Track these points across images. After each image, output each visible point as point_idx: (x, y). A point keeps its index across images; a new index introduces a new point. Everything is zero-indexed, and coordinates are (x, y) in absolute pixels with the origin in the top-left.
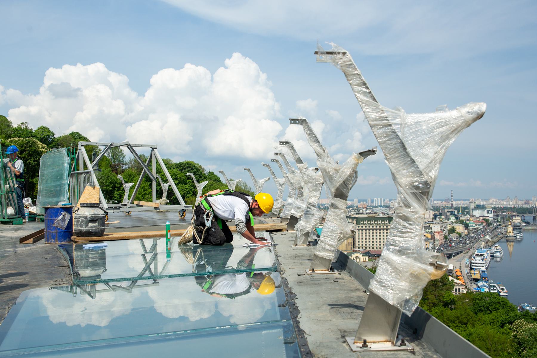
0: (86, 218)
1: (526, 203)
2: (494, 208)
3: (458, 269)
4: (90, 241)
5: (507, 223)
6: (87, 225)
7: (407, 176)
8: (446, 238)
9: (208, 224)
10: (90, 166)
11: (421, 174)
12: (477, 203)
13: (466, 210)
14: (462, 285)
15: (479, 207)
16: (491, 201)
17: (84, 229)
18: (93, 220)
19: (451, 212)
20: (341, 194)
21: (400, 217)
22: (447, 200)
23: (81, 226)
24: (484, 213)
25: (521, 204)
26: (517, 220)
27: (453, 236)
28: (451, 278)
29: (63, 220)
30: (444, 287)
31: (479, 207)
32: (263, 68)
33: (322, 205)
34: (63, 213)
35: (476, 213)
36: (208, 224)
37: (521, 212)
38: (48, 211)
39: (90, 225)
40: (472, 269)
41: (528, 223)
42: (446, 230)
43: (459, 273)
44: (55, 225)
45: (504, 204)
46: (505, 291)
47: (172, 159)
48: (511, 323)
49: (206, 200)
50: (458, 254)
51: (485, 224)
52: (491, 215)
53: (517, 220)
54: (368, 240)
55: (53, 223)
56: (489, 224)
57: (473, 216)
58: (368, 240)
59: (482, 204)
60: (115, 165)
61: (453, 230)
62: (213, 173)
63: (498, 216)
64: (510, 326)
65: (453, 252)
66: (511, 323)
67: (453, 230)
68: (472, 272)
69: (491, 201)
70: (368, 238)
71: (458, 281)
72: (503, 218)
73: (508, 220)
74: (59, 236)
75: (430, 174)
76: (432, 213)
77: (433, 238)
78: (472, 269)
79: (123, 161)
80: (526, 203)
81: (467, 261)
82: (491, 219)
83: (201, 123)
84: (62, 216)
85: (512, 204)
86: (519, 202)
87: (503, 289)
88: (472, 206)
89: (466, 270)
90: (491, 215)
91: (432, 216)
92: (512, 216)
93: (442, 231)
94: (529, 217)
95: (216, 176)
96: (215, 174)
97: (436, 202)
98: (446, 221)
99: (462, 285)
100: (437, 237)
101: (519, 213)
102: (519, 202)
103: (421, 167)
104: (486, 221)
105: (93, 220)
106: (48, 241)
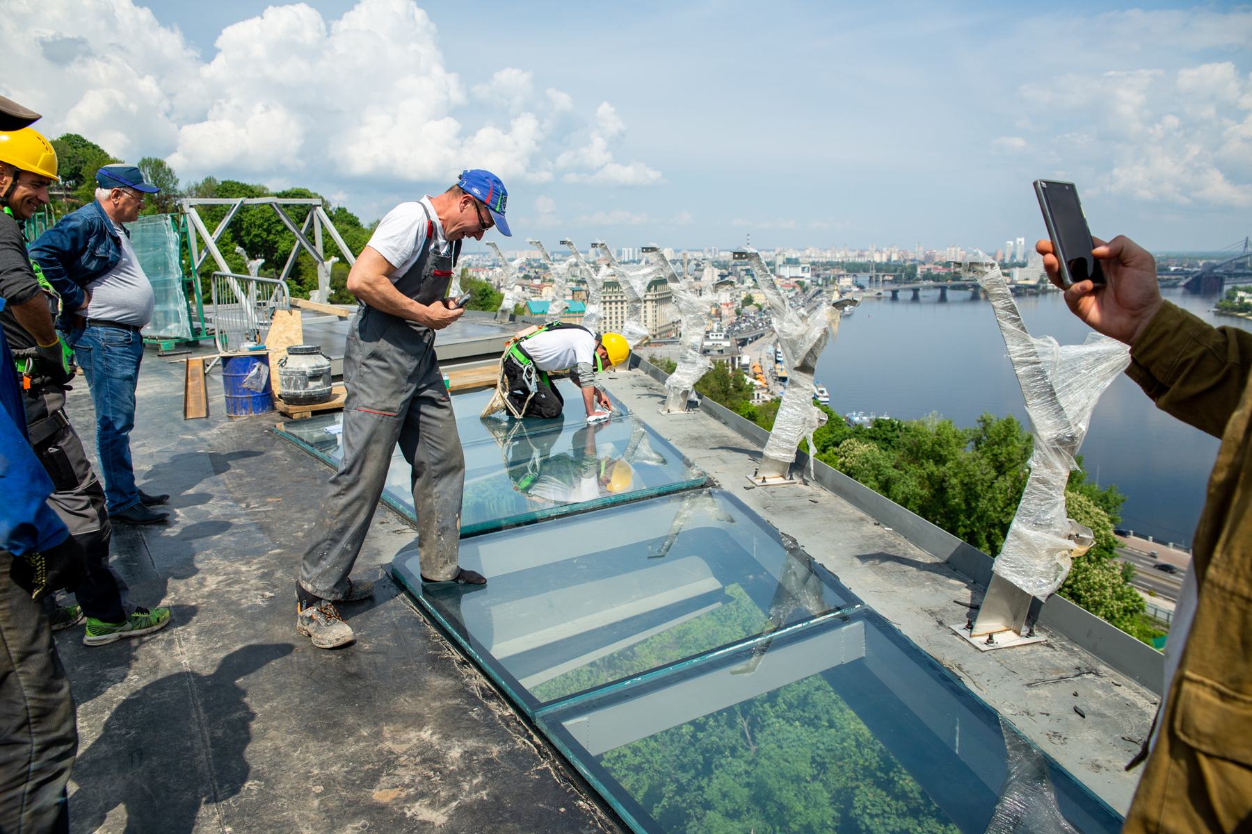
0: (304, 374)
1: (860, 256)
2: (813, 264)
3: (757, 363)
4: (314, 413)
5: (831, 287)
6: (306, 386)
7: (1051, 428)
8: (738, 313)
9: (533, 388)
10: (210, 241)
11: (1068, 425)
12: (788, 255)
14: (762, 388)
15: (791, 262)
16: (808, 252)
17: (301, 392)
18: (315, 377)
19: (747, 270)
20: (805, 368)
21: (1038, 480)
23: (296, 387)
24: (797, 271)
25: (852, 257)
26: (846, 282)
27: (750, 310)
28: (749, 380)
29: (258, 376)
30: (740, 394)
31: (791, 262)
32: (432, 17)
33: (535, 260)
34: (258, 364)
35: (786, 272)
36: (533, 388)
37: (853, 269)
38: (231, 362)
39: (312, 384)
40: (777, 362)
41: (861, 287)
42: (739, 301)
43: (758, 370)
44: (245, 386)
45: (828, 256)
46: (826, 394)
47: (266, 185)
48: (837, 444)
49: (519, 348)
50: (757, 338)
51: (798, 289)
52: (808, 275)
54: (614, 320)
55: (241, 383)
56: (805, 290)
57: (780, 277)
58: (614, 320)
59: (794, 256)
60: (160, 198)
61: (749, 301)
62: (344, 211)
63: (818, 276)
64: (836, 449)
65: (749, 336)
66: (837, 444)
67: (749, 301)
68: (778, 366)
69: (808, 252)
70: (614, 316)
71: (757, 383)
72: (826, 279)
73: (833, 283)
74: (254, 404)
75: (1080, 425)
76: (717, 272)
77: (719, 314)
78: (777, 362)
79: (175, 190)
80: (860, 256)
81: (771, 349)
82: (808, 282)
83: (320, 114)
84: (255, 370)
85: (838, 257)
86: (850, 254)
87: (822, 392)
88: (780, 260)
89: (769, 364)
90: (808, 275)
91: (717, 278)
92: (839, 276)
93: (732, 303)
94: (863, 278)
95: (351, 216)
96: (349, 211)
97: (722, 254)
98: (739, 285)
99: (762, 388)
100: (725, 312)
101: (849, 271)
102: (850, 254)
103: (1070, 417)
104: (801, 284)
105: (315, 377)
106: (235, 413)
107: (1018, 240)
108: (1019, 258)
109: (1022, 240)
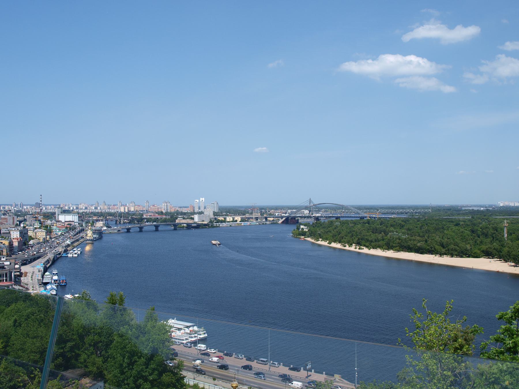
13: (51, 216)
22: (38, 205)
24: (69, 218)
35: (62, 218)
53: (99, 225)
57: (59, 221)
107: (201, 199)
108: (196, 210)
109: (203, 199)
